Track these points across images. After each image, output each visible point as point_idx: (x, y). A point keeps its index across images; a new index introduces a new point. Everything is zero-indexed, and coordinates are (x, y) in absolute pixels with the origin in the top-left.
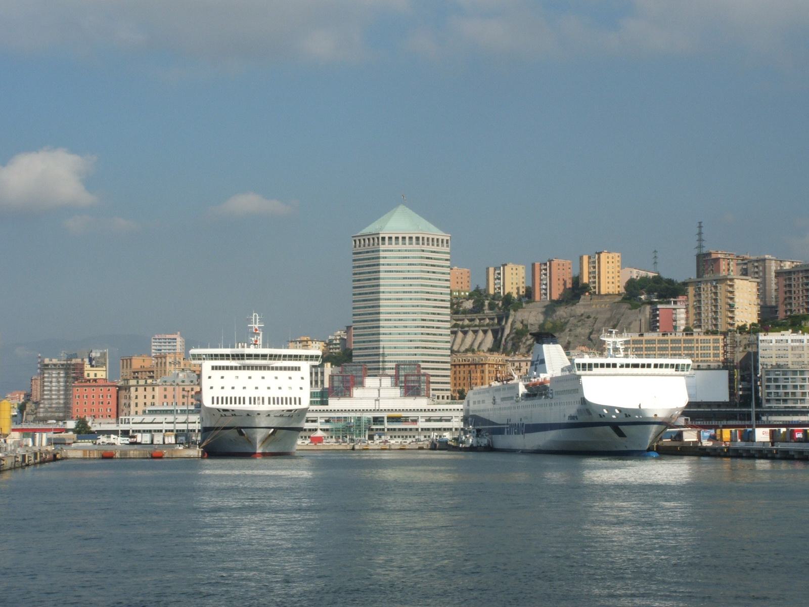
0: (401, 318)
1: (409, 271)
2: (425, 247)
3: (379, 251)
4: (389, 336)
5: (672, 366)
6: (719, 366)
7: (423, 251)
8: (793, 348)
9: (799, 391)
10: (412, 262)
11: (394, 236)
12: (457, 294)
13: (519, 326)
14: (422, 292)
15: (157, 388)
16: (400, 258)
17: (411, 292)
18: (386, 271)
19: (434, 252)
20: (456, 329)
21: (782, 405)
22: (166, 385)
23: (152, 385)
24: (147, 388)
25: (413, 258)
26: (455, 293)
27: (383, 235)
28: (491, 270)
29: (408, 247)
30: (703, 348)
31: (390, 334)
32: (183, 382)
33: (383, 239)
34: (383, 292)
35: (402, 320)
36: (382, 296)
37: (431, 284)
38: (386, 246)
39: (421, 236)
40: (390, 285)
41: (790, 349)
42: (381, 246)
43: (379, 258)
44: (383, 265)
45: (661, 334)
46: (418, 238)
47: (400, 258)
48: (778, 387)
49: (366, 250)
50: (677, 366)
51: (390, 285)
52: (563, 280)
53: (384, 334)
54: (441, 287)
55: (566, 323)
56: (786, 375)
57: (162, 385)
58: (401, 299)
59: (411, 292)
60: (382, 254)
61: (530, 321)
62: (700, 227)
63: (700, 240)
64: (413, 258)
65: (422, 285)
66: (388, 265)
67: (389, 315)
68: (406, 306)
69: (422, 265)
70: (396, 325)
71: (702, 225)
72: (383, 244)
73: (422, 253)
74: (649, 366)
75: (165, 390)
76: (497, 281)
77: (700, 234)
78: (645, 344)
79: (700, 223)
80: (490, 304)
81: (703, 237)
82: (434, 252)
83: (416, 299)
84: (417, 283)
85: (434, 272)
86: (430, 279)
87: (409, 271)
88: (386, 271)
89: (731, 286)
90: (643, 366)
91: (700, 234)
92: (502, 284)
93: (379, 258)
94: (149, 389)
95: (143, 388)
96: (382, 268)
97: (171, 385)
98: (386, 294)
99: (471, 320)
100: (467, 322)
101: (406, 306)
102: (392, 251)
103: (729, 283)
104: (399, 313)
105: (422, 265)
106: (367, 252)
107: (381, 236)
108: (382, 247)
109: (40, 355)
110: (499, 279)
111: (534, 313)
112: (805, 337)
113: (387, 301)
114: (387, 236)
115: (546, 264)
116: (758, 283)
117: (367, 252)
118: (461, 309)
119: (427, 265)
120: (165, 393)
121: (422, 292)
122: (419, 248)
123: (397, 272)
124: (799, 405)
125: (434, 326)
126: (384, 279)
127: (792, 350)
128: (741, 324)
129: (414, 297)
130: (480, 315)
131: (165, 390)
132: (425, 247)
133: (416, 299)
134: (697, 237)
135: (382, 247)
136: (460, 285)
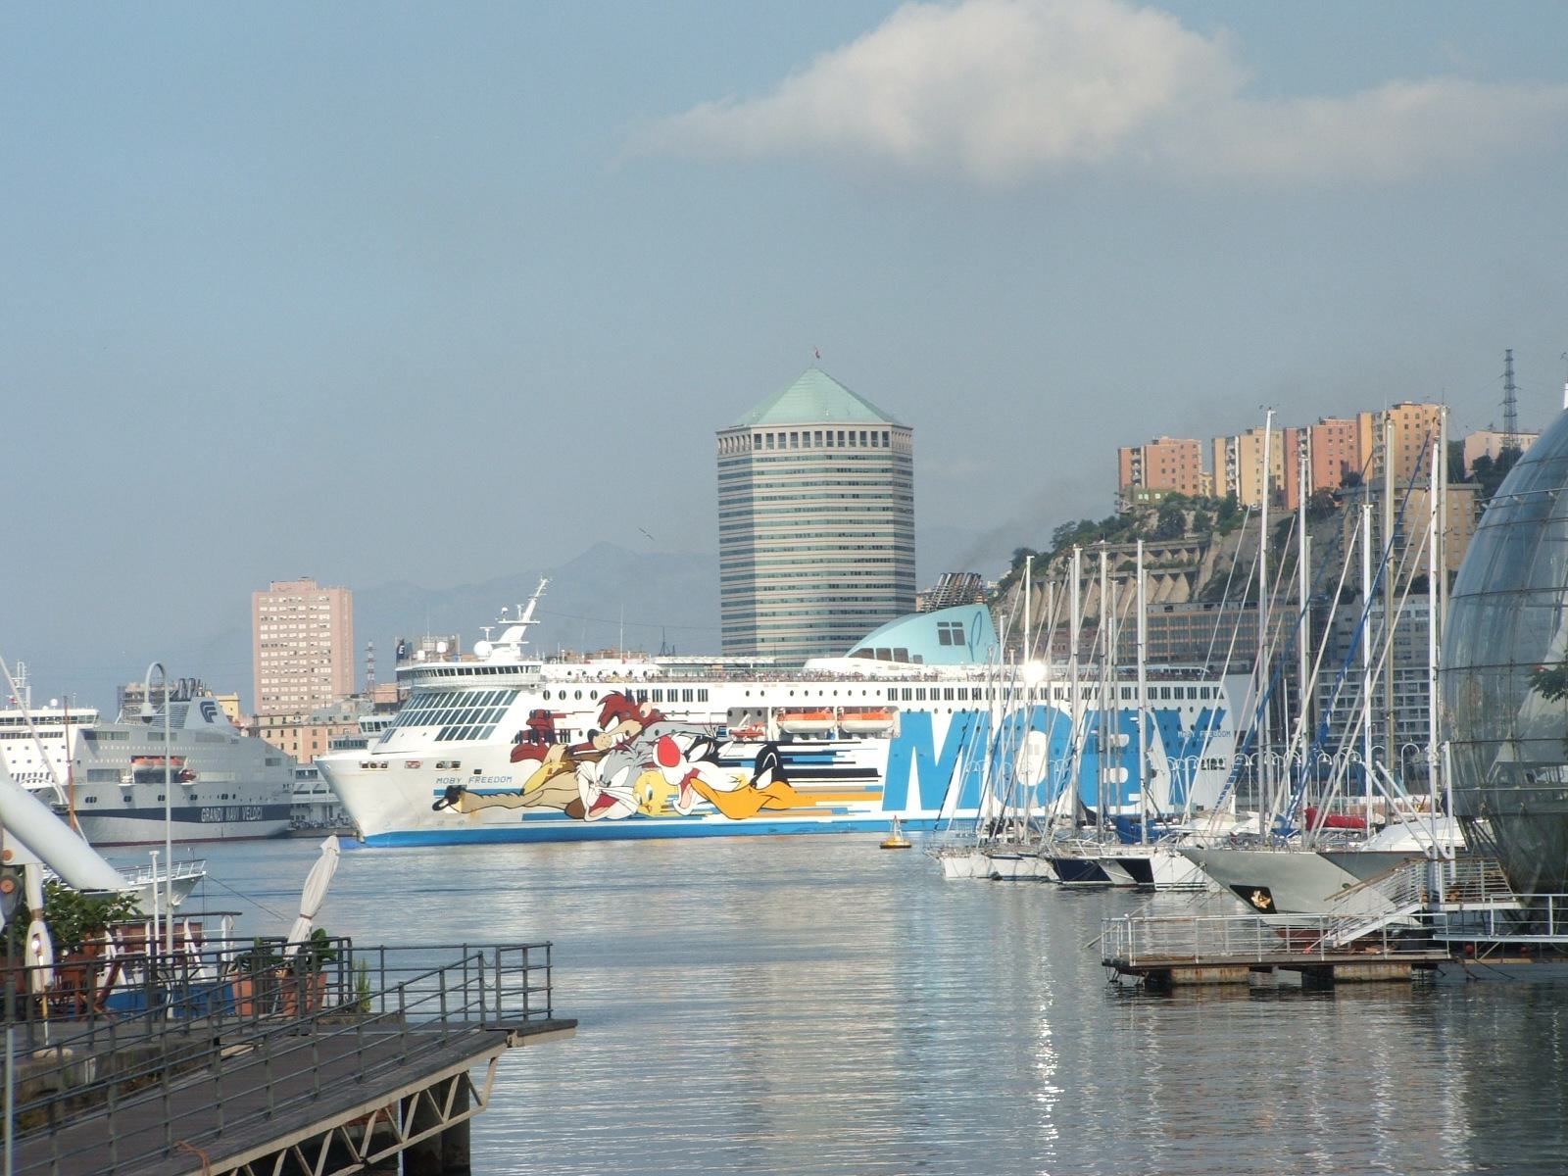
0: (792, 584)
1: (804, 497)
2: (835, 450)
3: (750, 461)
4: (772, 618)
6: (1244, 666)
7: (830, 457)
10: (810, 480)
11: (776, 432)
12: (1147, 497)
14: (829, 535)
15: (300, 731)
16: (787, 472)
17: (809, 535)
18: (763, 499)
19: (856, 458)
20: (1124, 574)
22: (315, 725)
23: (293, 725)
24: (286, 731)
25: (812, 471)
26: (1140, 497)
27: (757, 432)
28: (1220, 444)
31: (774, 614)
32: (346, 718)
33: (758, 437)
34: (760, 537)
35: (794, 587)
37: (849, 518)
38: (765, 451)
39: (847, 430)
40: (772, 524)
41: (1413, 628)
42: (754, 451)
44: (759, 486)
45: (1202, 605)
46: (818, 434)
47: (787, 472)
49: (735, 459)
51: (772, 524)
52: (1342, 462)
53: (762, 615)
54: (873, 522)
56: (1354, 680)
57: (309, 725)
58: (792, 549)
59: (809, 535)
62: (1509, 360)
63: (1510, 387)
64: (812, 471)
65: (828, 522)
66: (767, 486)
67: (771, 579)
68: (801, 562)
69: (828, 483)
70: (783, 597)
71: (1513, 355)
72: (759, 447)
73: (829, 461)
75: (315, 733)
76: (1231, 466)
77: (1509, 374)
78: (1171, 625)
79: (1509, 351)
80: (1196, 518)
82: (856, 458)
83: (817, 549)
84: (860, 505)
85: (855, 496)
86: (846, 509)
87: (804, 497)
88: (763, 499)
91: (1509, 374)
92: (1237, 473)
94: (288, 732)
95: (279, 731)
97: (324, 725)
98: (766, 541)
101: (801, 562)
102: (774, 460)
104: (790, 575)
105: (828, 483)
106: (737, 462)
107: (753, 432)
108: (756, 454)
109: (370, 644)
110: (1139, 481)
113: (766, 554)
115: (1305, 431)
116: (1476, 491)
117: (737, 462)
118: (1145, 529)
119: (839, 483)
120: (315, 739)
121: (829, 535)
122: (821, 454)
123: (783, 498)
125: (858, 595)
126: (760, 512)
127: (1417, 630)
129: (815, 544)
130: (1173, 543)
131: (315, 733)
132: (835, 450)
133: (817, 549)
134: (1503, 381)
135: (756, 454)
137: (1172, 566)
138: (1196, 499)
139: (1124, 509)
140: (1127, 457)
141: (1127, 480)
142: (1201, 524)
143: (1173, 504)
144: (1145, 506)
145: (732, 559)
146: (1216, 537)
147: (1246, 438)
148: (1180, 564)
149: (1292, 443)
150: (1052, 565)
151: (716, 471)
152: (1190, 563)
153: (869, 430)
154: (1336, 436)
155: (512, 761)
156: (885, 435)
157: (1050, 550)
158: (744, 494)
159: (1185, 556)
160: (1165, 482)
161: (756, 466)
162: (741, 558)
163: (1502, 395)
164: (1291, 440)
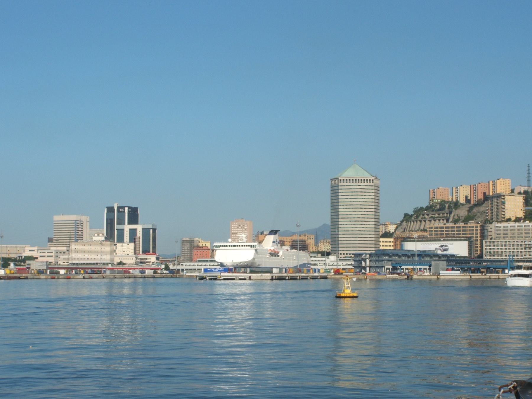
2: (360, 184)
5: (249, 246)
8: (511, 230)
9: (500, 251)
13: (456, 217)
21: (492, 257)
29: (351, 184)
30: (470, 230)
33: (341, 180)
36: (340, 207)
38: (342, 184)
43: (338, 189)
48: (490, 249)
50: (251, 246)
55: (476, 216)
60: (340, 187)
61: (461, 215)
62: (529, 166)
63: (529, 173)
74: (240, 246)
77: (529, 170)
80: (449, 206)
81: (530, 172)
89: (504, 199)
90: (237, 246)
91: (529, 170)
93: (338, 189)
96: (340, 194)
99: (439, 214)
100: (437, 215)
103: (503, 197)
108: (340, 184)
111: (464, 211)
112: (530, 224)
114: (342, 179)
124: (500, 257)
128: (508, 217)
130: (443, 212)
132: (360, 184)
135: (340, 184)
136: (442, 196)
137: (443, 217)
138: (448, 202)
139: (431, 204)
140: (432, 192)
141: (431, 197)
142: (449, 207)
143: (443, 203)
144: (437, 203)
145: (333, 211)
146: (454, 210)
147: (461, 187)
148: (444, 217)
149: (474, 189)
150: (413, 217)
151: (330, 189)
152: (447, 217)
153: (368, 179)
154: (483, 186)
155: (137, 208)
156: (373, 180)
157: (413, 214)
158: (336, 207)
159: (446, 215)
160: (441, 198)
161: (340, 187)
162: (336, 210)
163: (527, 175)
164: (472, 187)
